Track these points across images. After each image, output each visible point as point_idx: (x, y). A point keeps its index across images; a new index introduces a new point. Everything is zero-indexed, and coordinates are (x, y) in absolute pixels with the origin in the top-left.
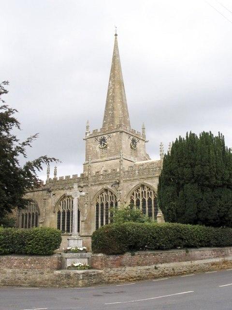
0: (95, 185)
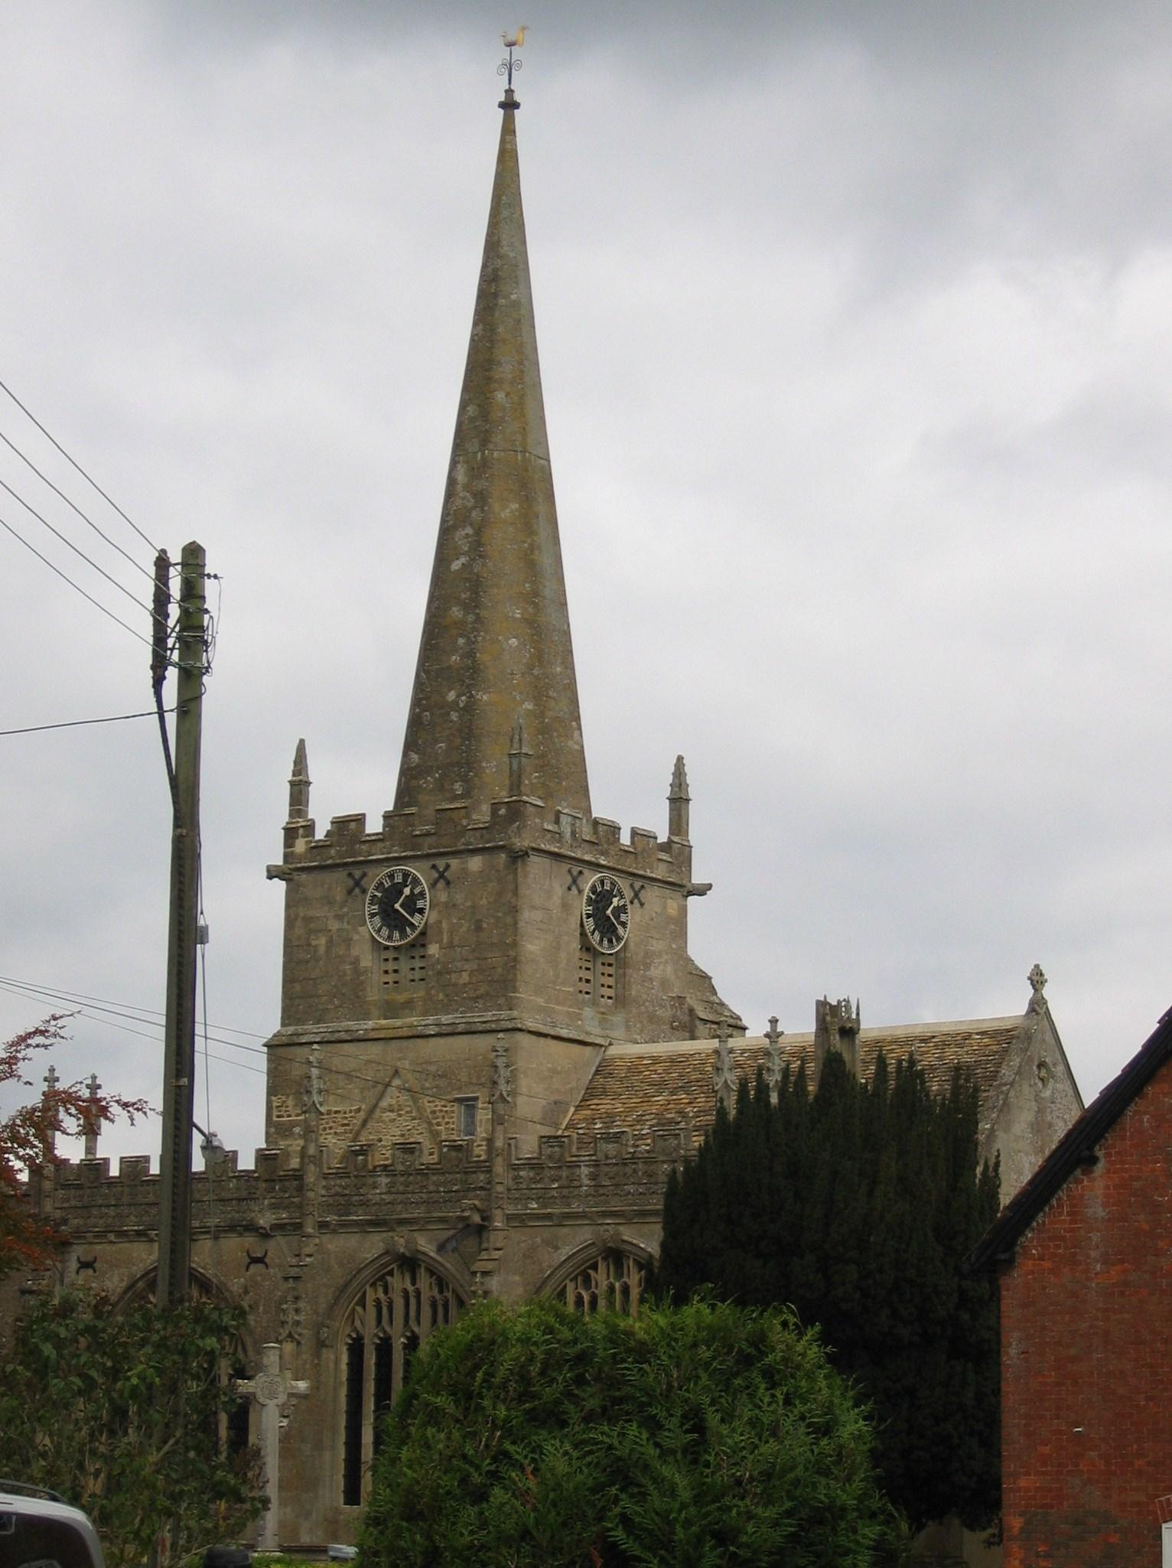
0: (344, 1225)
